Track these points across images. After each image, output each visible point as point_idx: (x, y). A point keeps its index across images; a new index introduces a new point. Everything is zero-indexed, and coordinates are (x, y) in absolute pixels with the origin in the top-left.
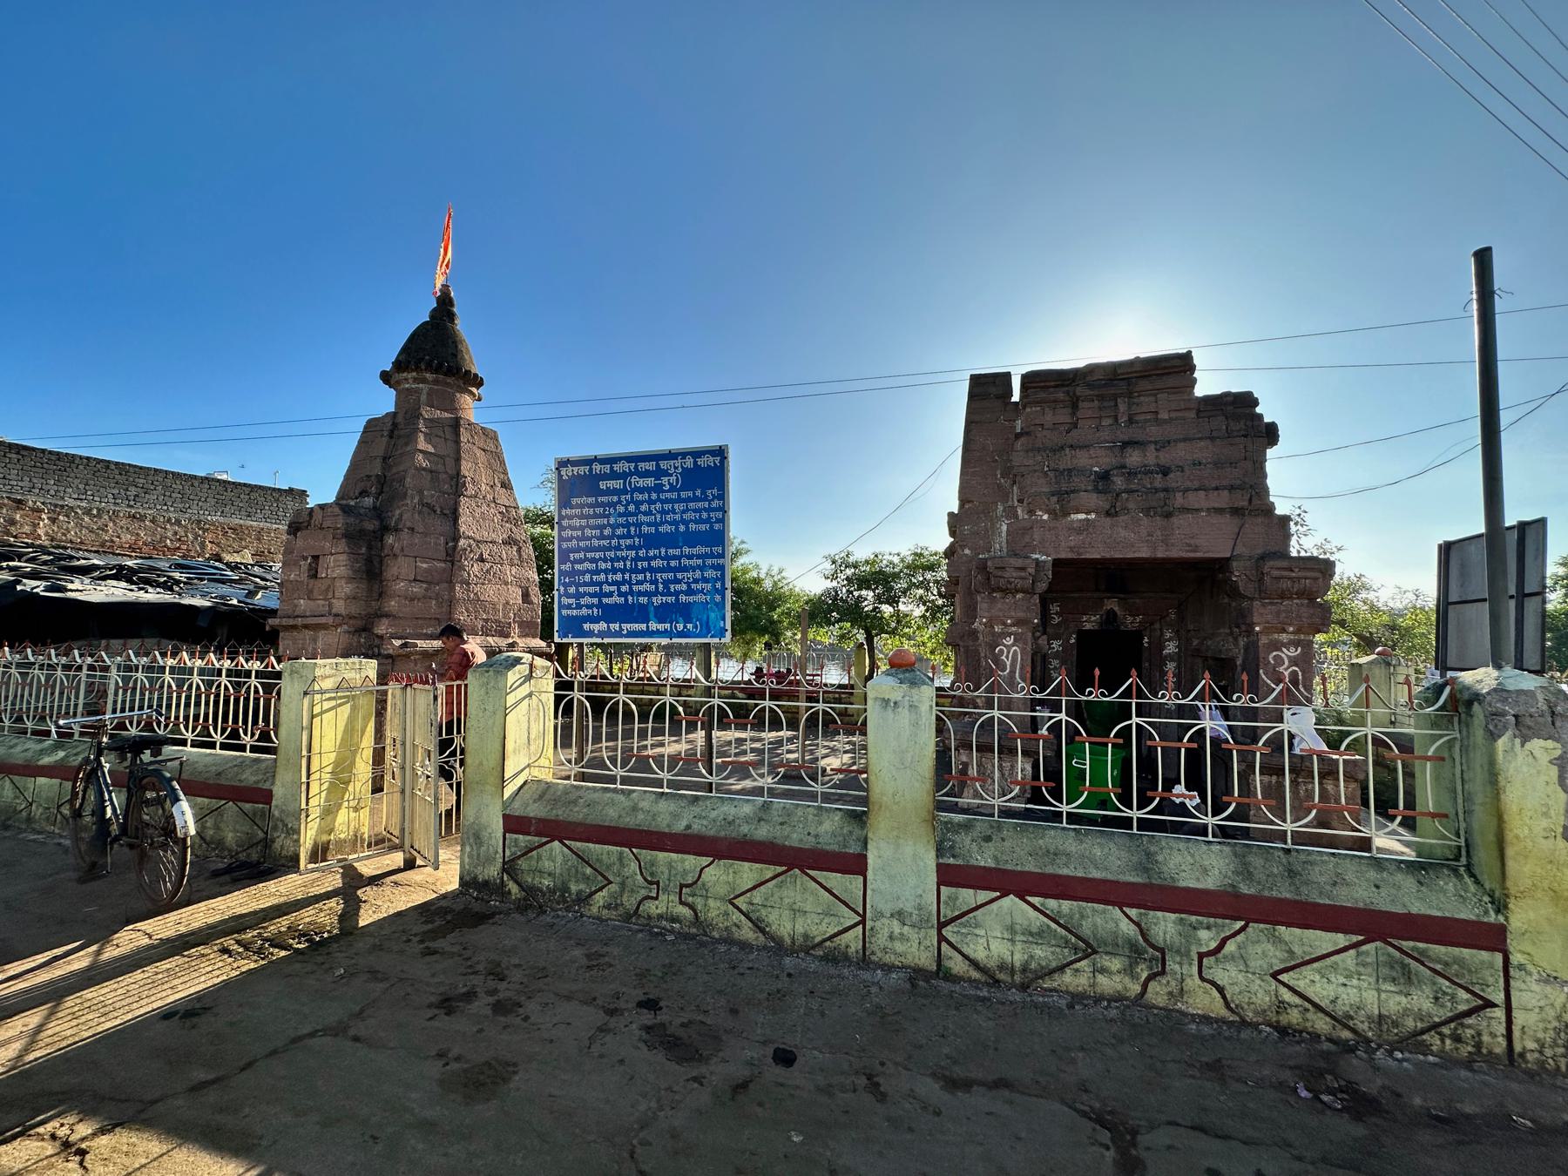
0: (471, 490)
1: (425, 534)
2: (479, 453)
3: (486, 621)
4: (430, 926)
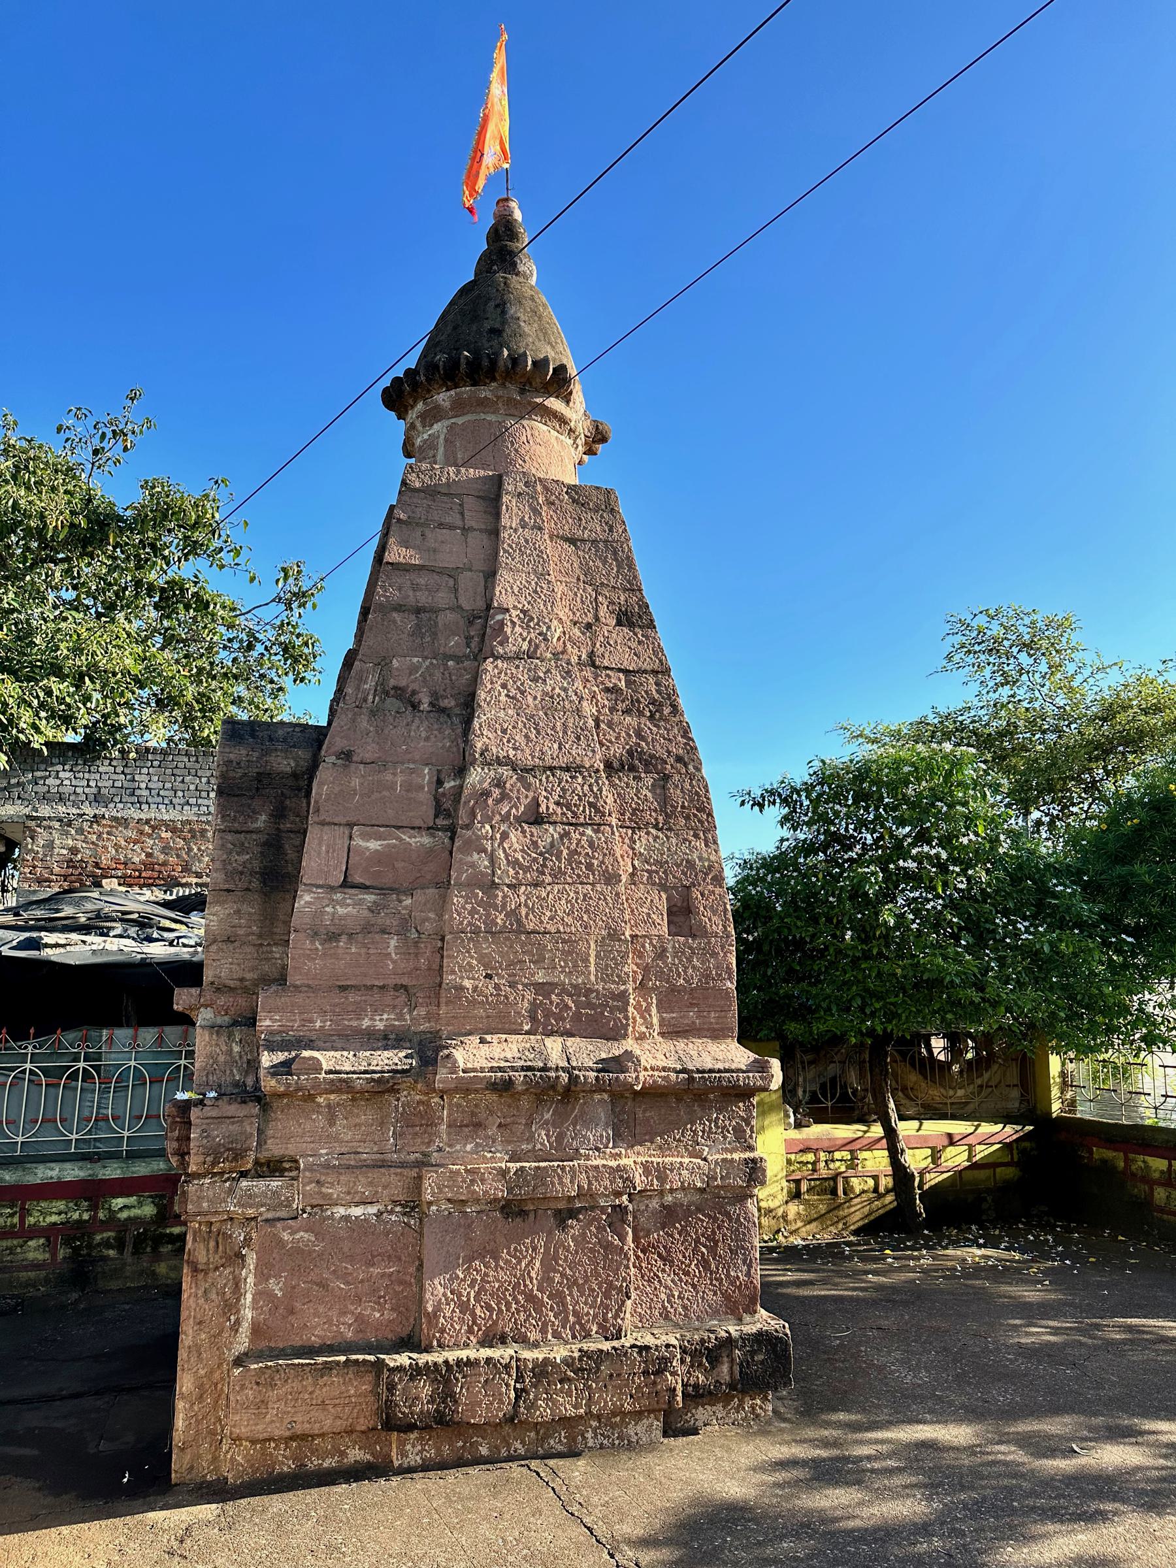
0: (517, 638)
1: (379, 764)
2: (551, 549)
3: (543, 989)
4: (1162, 1462)
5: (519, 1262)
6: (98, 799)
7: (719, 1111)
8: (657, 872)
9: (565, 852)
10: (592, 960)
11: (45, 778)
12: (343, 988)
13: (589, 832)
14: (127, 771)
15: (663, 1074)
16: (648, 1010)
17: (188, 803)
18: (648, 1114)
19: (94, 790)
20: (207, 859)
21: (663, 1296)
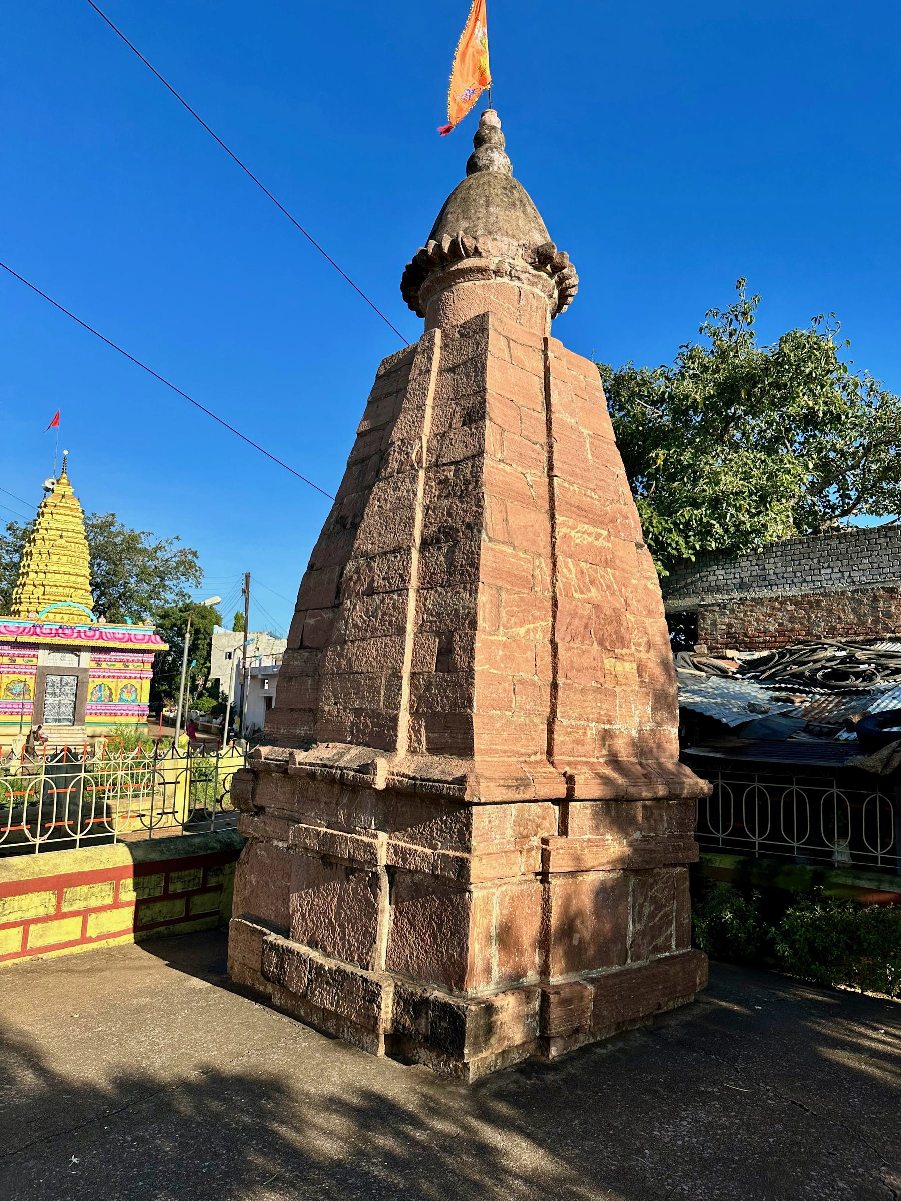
5: (327, 897)
6: (742, 586)
7: (449, 814)
8: (435, 622)
9: (380, 613)
10: (382, 693)
11: (707, 576)
12: (292, 710)
13: (395, 597)
14: (760, 563)
15: (400, 778)
16: (419, 730)
17: (805, 581)
18: (404, 809)
19: (739, 581)
20: (823, 624)
21: (408, 952)
